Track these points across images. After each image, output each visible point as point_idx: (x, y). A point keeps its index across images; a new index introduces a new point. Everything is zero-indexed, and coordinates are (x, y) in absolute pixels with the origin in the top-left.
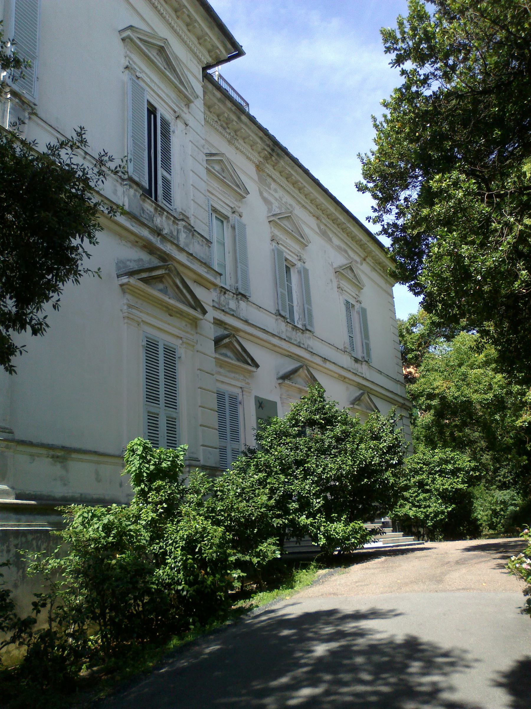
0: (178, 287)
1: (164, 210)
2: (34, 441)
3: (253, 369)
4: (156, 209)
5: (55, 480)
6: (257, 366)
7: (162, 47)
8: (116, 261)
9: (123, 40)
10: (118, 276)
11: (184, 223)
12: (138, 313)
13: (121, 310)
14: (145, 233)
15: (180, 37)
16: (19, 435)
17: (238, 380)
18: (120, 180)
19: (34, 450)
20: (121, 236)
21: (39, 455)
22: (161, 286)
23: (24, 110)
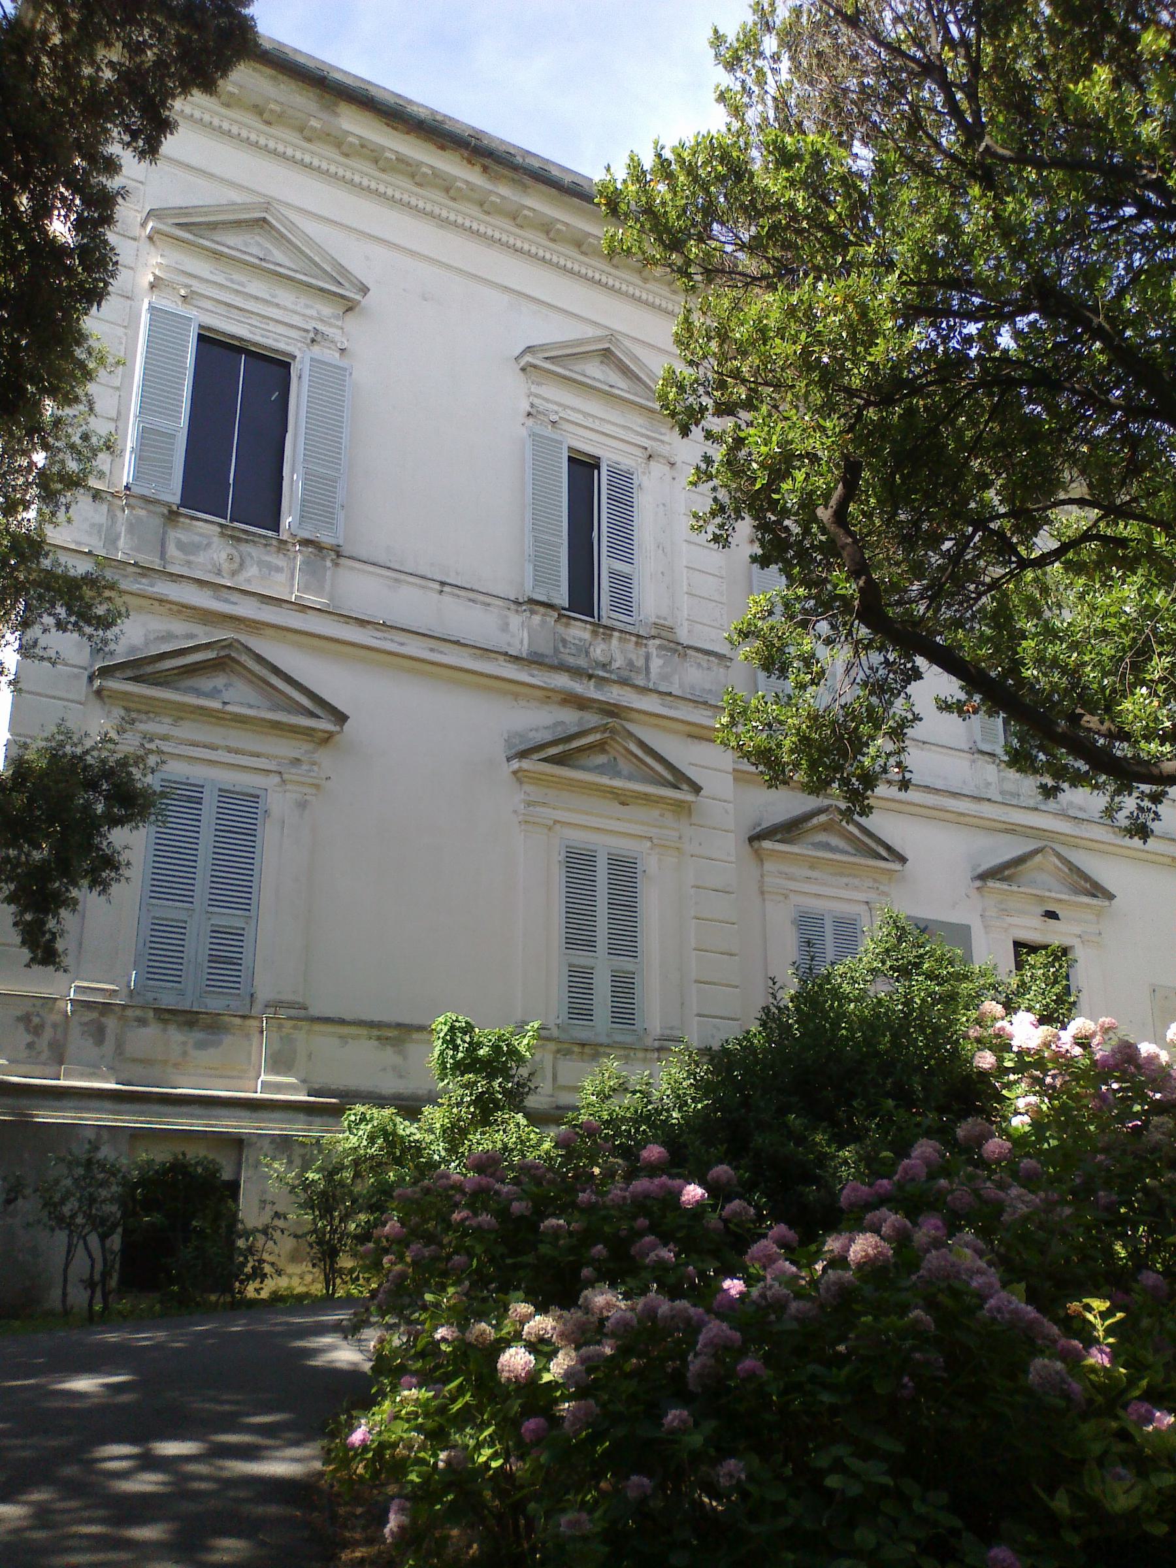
0: (636, 756)
1: (613, 629)
2: (348, 1017)
3: (896, 866)
4: (595, 633)
5: (384, 1069)
6: (903, 860)
7: (607, 350)
8: (506, 736)
9: (523, 369)
10: (509, 759)
11: (657, 642)
12: (549, 811)
13: (515, 812)
14: (562, 681)
15: (653, 305)
16: (314, 1011)
17: (856, 888)
18: (513, 607)
19: (345, 1030)
20: (516, 696)
21: (355, 1037)
22: (601, 759)
23: (323, 559)
